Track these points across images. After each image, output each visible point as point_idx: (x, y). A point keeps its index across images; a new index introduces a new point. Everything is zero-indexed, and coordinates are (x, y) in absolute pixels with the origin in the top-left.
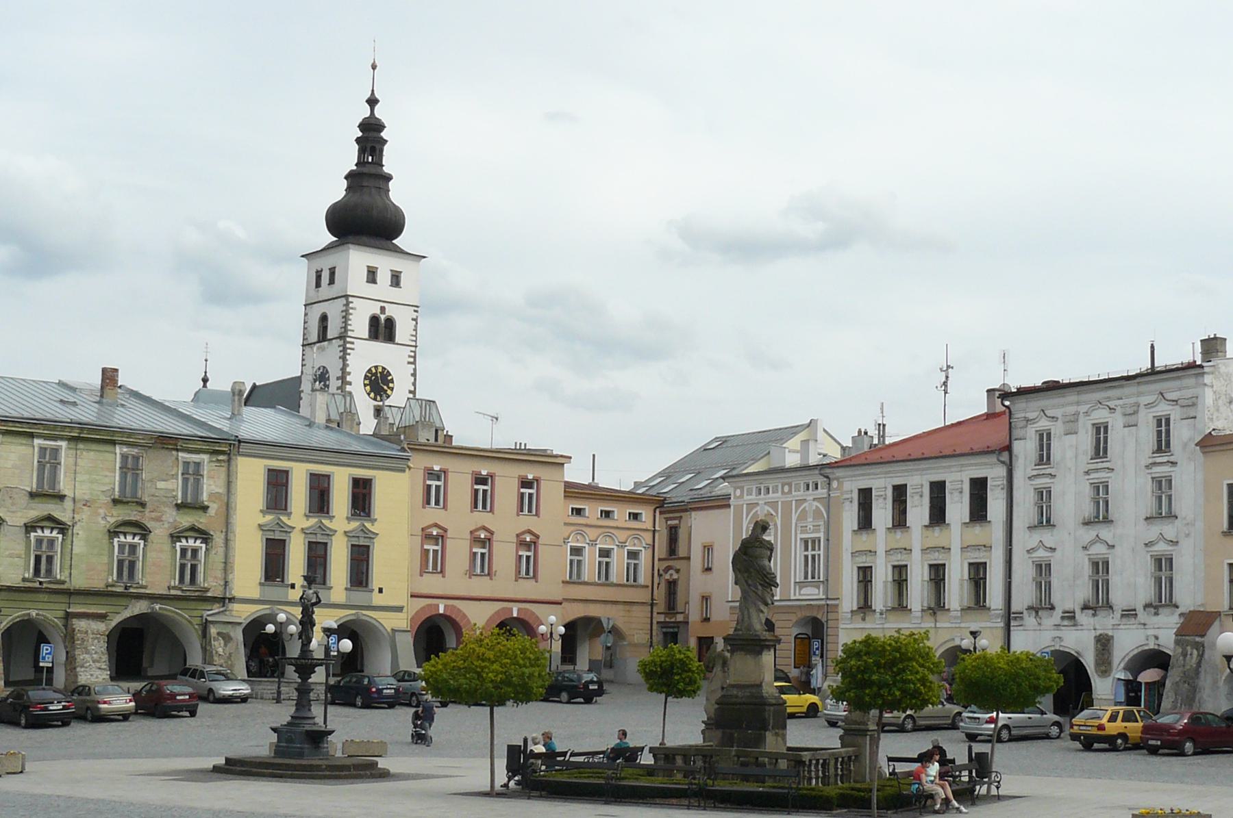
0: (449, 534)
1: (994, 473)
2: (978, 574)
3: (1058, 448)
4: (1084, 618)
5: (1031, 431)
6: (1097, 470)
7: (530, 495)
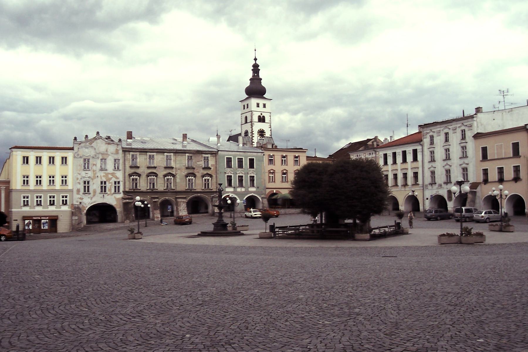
0: (276, 172)
1: (419, 148)
2: (416, 175)
3: (436, 140)
4: (444, 186)
5: (428, 136)
6: (446, 145)
7: (285, 160)
